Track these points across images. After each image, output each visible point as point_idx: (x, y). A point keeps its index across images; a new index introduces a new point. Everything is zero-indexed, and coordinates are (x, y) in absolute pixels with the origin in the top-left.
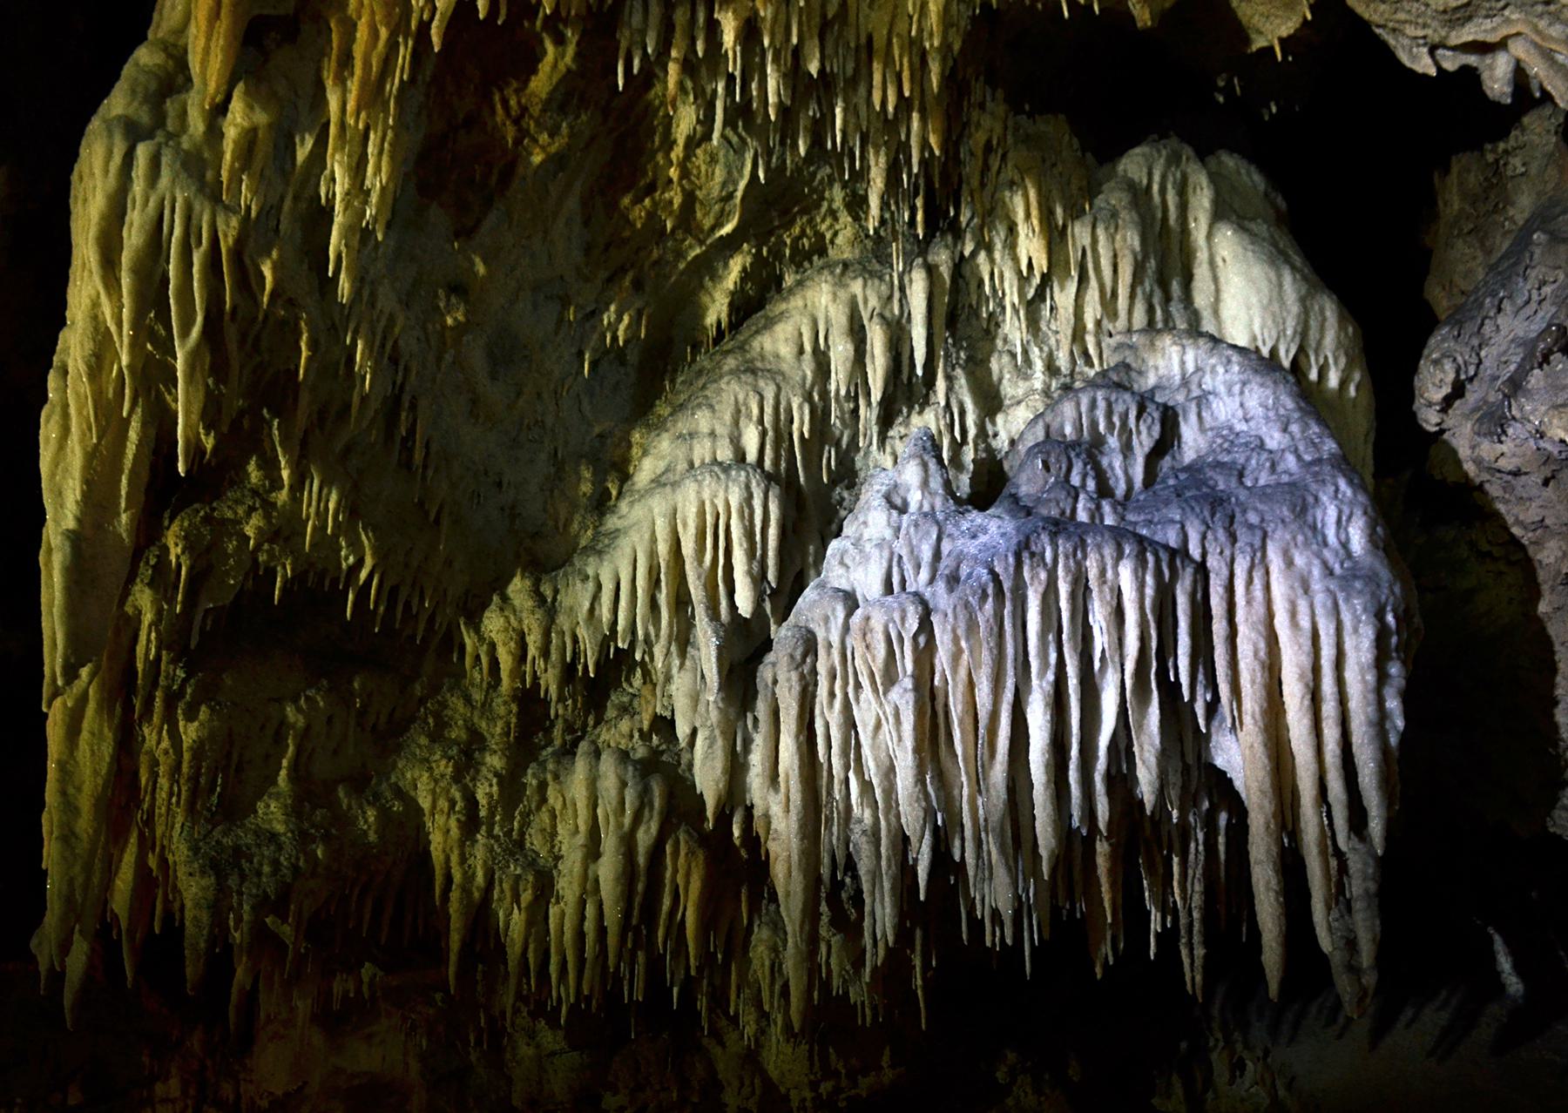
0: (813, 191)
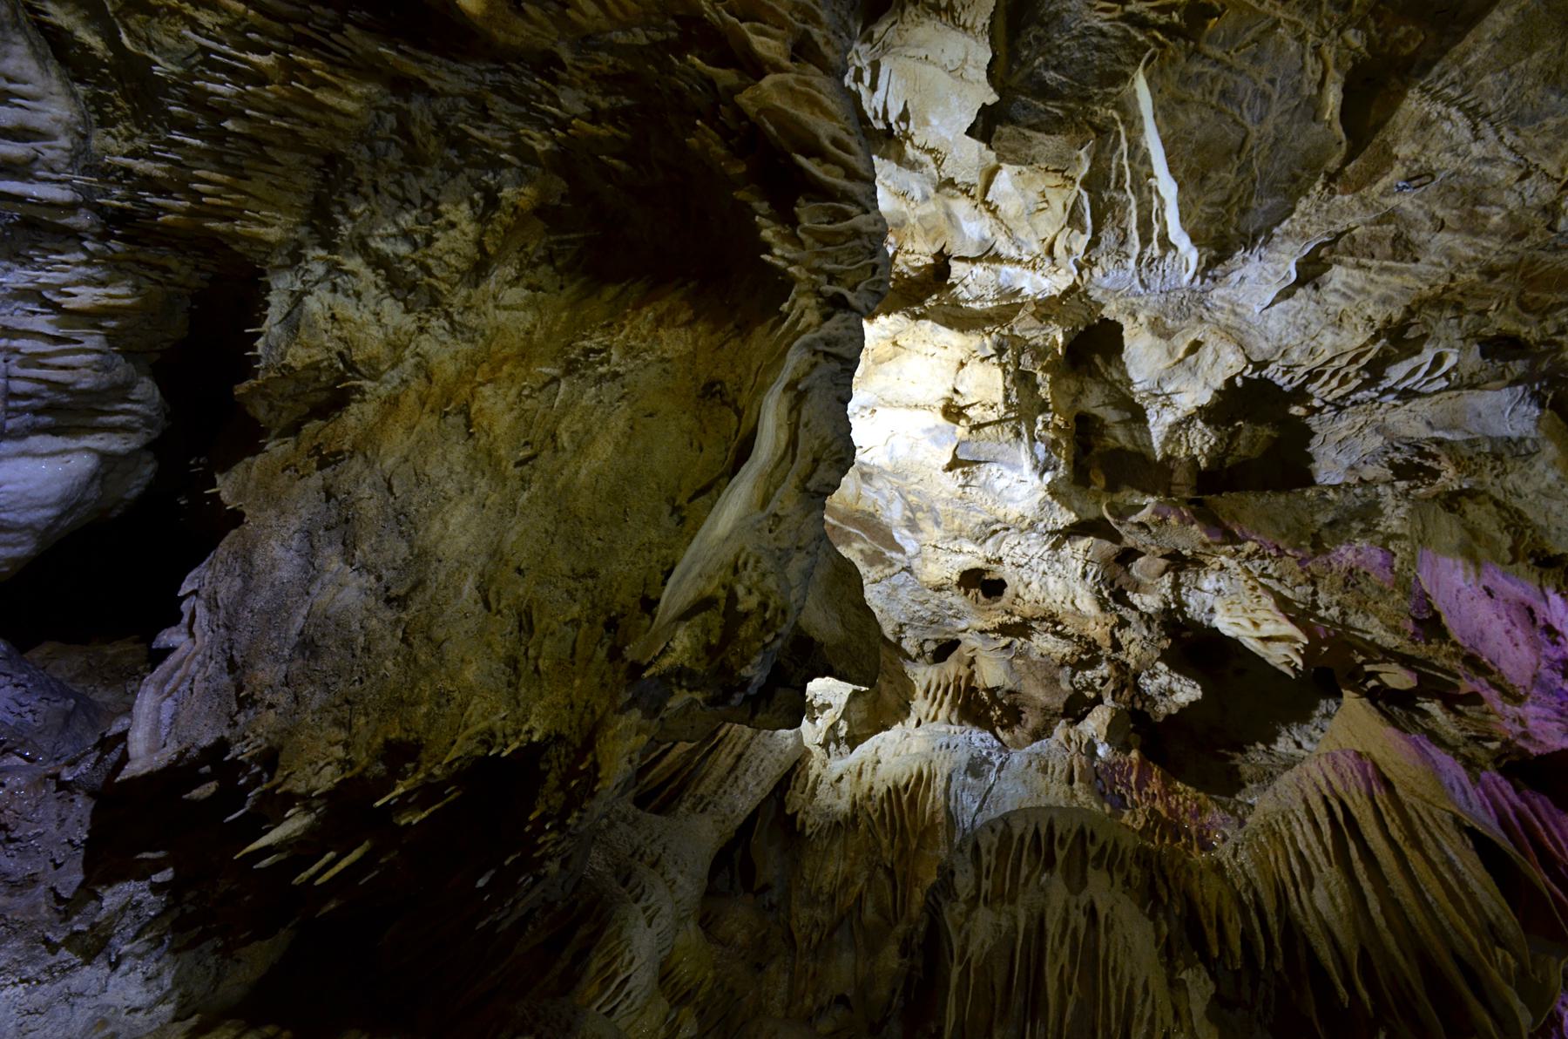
0: (149, 124)
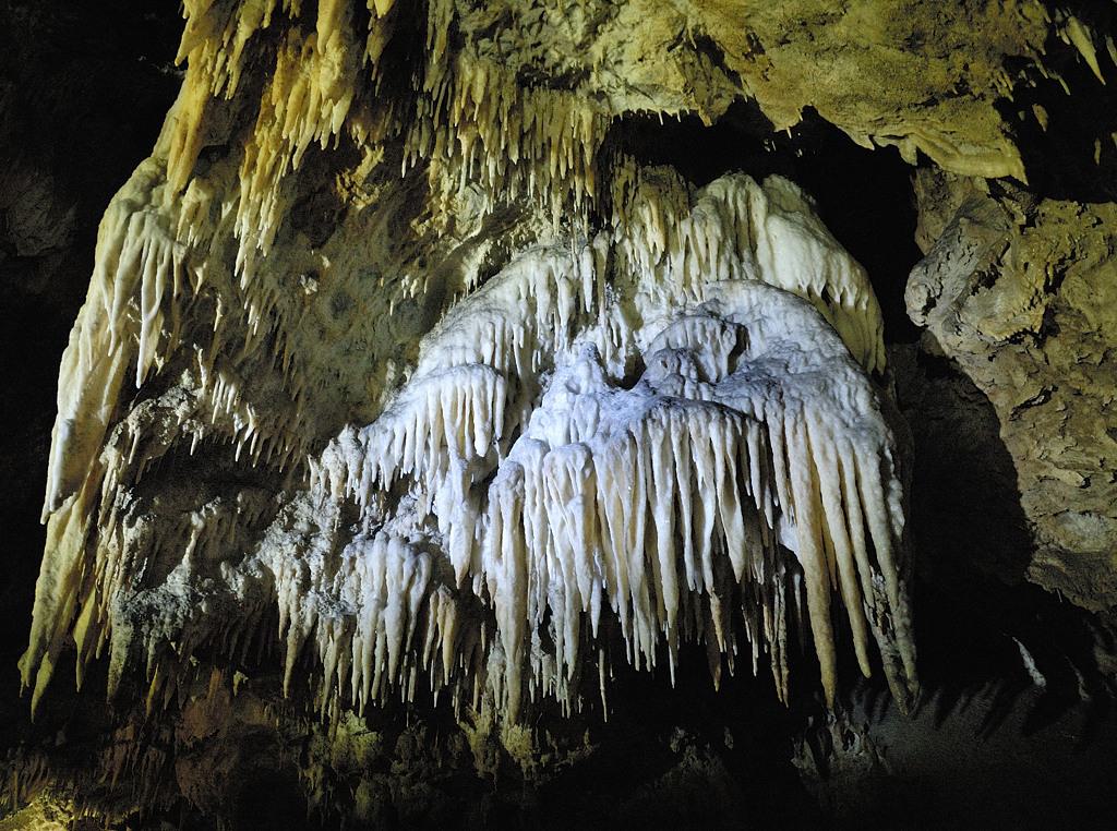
0: (527, 210)
